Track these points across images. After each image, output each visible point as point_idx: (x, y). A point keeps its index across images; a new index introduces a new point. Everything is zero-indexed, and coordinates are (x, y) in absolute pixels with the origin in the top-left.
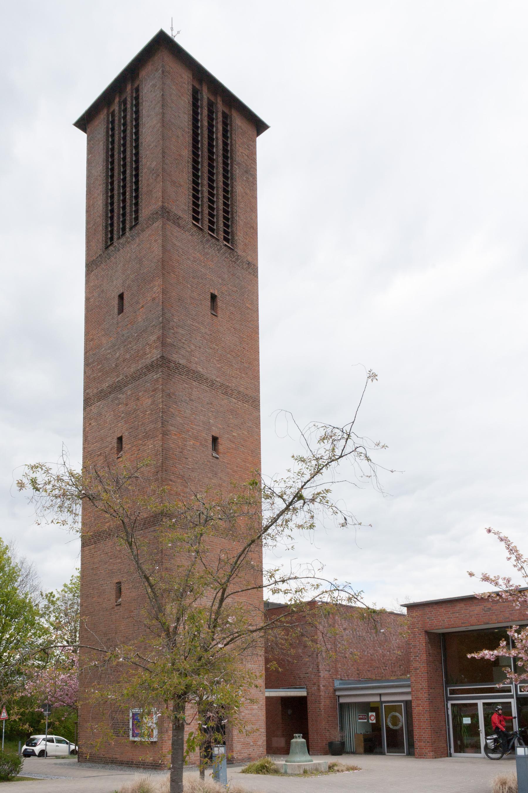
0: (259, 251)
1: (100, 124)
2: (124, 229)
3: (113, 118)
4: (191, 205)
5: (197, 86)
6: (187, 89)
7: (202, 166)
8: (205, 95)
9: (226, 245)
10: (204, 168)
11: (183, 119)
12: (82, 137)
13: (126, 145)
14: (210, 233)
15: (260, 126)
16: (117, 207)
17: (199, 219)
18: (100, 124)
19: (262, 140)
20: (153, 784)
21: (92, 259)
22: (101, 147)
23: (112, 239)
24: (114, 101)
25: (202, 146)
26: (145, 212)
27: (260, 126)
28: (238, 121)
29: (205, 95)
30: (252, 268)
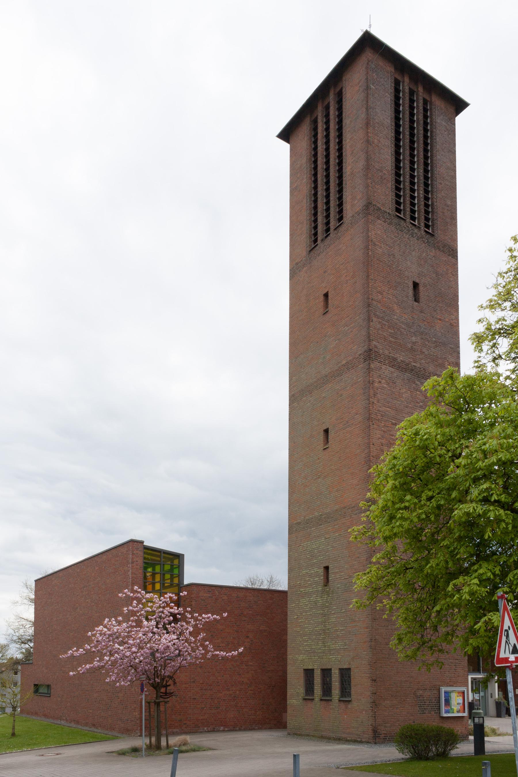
0: (457, 202)
1: (305, 129)
2: (328, 230)
3: (316, 124)
4: (393, 175)
5: (399, 78)
6: (389, 86)
7: (404, 178)
8: (406, 85)
9: (425, 231)
10: (405, 142)
11: (384, 115)
12: (285, 147)
13: (329, 169)
14: (412, 222)
15: (459, 105)
16: (320, 208)
17: (401, 210)
18: (305, 129)
19: (460, 119)
20: (364, 334)
21: (292, 393)
22: (304, 160)
23: (315, 241)
24: (317, 107)
25: (404, 151)
26: (349, 210)
27: (459, 105)
28: (438, 103)
29: (406, 85)
30: (451, 252)
